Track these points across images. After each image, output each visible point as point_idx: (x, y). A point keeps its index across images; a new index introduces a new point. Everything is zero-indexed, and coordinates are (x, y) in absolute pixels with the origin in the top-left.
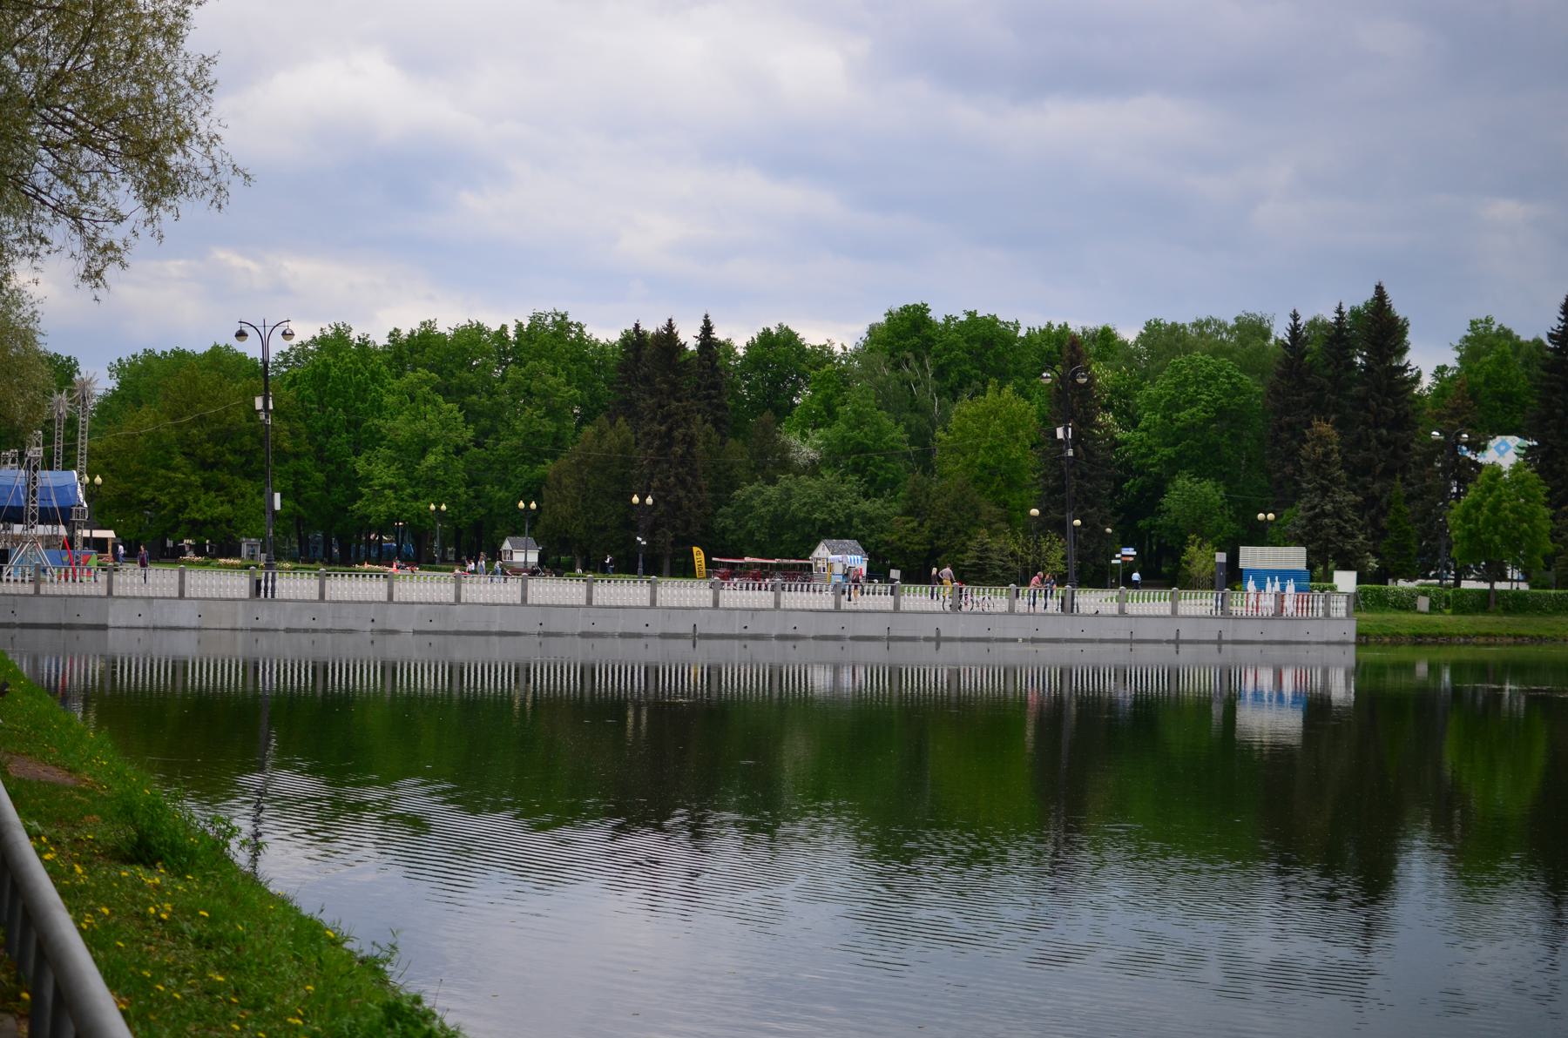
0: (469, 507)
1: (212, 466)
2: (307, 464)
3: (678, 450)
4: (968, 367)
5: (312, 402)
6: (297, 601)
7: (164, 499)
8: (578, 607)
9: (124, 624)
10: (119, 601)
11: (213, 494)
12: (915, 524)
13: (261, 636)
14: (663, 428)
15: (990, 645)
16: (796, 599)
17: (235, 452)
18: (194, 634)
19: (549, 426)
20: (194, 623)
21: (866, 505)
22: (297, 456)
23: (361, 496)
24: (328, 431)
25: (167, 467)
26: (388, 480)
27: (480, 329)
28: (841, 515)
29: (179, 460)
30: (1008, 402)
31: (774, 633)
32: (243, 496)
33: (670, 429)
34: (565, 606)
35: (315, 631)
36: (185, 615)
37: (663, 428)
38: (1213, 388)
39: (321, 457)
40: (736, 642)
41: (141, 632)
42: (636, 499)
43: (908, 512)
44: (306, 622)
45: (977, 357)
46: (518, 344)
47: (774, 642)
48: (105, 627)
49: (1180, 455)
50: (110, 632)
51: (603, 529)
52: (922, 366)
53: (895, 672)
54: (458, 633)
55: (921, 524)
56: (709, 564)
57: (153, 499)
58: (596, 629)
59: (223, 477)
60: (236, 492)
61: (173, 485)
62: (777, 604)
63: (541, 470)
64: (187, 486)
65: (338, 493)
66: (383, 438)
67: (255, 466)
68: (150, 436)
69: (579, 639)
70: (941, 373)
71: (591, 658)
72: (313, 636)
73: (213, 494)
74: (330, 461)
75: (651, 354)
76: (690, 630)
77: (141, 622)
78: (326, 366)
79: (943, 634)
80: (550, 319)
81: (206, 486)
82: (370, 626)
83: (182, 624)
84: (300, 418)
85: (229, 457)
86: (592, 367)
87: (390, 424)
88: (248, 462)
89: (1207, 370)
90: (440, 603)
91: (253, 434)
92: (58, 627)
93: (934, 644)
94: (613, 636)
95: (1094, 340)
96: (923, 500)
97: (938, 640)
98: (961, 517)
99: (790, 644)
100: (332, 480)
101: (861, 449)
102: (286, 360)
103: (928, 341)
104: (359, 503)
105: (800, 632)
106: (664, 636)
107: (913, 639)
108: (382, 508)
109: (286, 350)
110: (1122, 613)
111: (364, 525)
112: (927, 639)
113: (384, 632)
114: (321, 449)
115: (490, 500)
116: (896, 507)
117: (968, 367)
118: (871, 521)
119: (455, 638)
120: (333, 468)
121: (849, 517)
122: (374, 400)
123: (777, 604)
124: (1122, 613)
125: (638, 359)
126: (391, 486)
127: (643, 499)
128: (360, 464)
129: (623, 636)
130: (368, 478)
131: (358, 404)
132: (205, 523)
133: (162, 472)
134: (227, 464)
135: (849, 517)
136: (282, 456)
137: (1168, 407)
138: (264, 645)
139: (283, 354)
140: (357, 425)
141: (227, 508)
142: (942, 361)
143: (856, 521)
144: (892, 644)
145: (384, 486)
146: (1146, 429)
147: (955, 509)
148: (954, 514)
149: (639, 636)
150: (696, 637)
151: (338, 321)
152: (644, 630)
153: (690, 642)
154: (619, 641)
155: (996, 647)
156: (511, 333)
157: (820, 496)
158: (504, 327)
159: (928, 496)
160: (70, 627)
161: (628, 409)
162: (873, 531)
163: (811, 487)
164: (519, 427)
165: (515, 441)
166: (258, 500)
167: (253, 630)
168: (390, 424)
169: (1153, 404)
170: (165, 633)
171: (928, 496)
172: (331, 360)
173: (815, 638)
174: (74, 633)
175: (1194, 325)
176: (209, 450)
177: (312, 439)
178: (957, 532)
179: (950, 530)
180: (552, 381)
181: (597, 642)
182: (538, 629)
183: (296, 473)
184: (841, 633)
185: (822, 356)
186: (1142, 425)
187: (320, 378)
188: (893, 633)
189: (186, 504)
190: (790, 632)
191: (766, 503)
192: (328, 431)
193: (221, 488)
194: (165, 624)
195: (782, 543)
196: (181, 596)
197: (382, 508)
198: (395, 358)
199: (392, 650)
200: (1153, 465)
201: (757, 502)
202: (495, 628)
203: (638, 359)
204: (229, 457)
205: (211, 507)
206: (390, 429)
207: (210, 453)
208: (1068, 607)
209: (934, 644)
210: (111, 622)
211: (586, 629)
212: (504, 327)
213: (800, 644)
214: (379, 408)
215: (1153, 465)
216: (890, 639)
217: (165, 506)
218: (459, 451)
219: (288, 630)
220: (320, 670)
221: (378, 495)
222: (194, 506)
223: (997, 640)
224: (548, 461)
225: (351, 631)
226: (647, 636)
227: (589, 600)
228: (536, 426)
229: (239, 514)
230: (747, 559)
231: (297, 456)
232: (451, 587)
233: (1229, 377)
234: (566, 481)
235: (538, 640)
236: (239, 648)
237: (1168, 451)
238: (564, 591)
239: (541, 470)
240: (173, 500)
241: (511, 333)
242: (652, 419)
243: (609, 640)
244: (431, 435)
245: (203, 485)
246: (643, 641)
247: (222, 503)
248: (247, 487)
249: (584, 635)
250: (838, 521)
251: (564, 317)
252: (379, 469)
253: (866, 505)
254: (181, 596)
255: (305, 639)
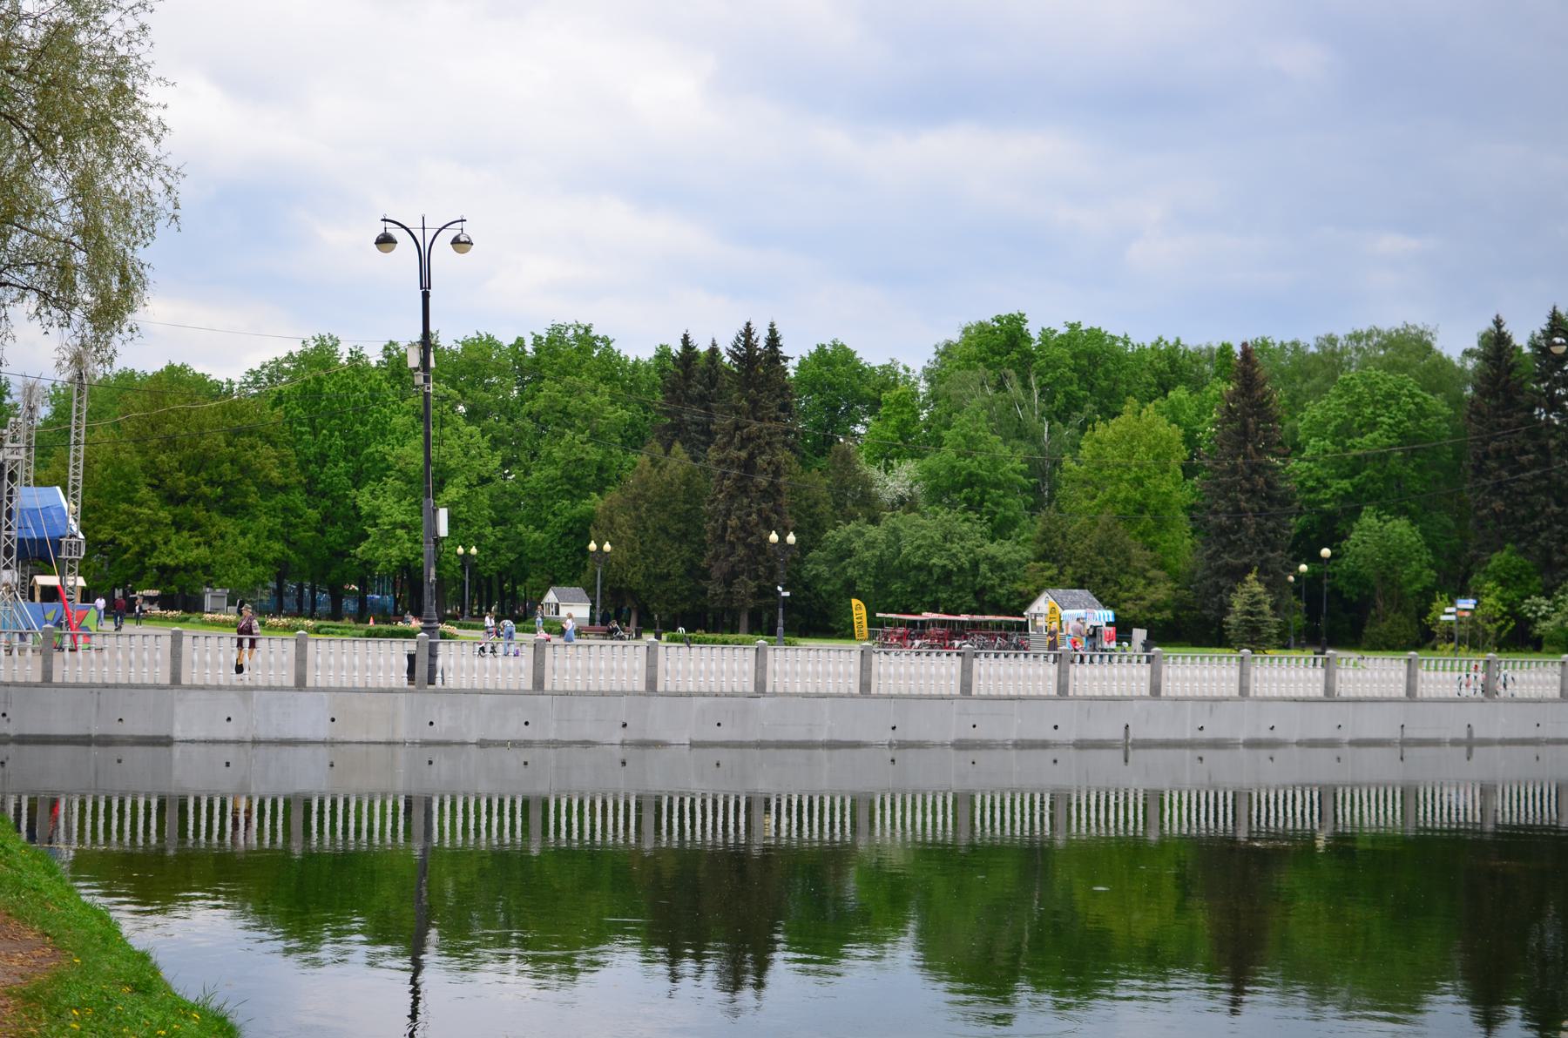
0: (495, 551)
1: (183, 500)
2: (297, 498)
3: (763, 481)
4: (1075, 387)
5: (301, 424)
6: (497, 692)
7: (126, 540)
8: (950, 698)
9: (202, 735)
10: (193, 694)
11: (186, 534)
12: (1055, 571)
13: (438, 754)
14: (743, 454)
15: (1540, 750)
16: (999, 672)
17: (211, 483)
18: (323, 751)
19: (594, 454)
20: (324, 732)
21: (992, 549)
22: (284, 489)
23: (366, 536)
24: (322, 459)
25: (130, 501)
26: (400, 518)
27: (491, 343)
28: (964, 560)
29: (144, 492)
30: (1147, 424)
31: (1242, 736)
32: (222, 537)
33: (751, 456)
34: (931, 697)
35: (527, 744)
36: (307, 718)
37: (743, 454)
38: (1394, 409)
39: (310, 488)
40: (1188, 752)
41: (232, 749)
42: (593, 546)
43: (1042, 557)
44: (513, 731)
45: (1084, 376)
46: (536, 361)
47: (1242, 751)
48: (167, 741)
49: (1359, 489)
50: (177, 750)
51: (666, 577)
52: (1026, 386)
53: (1409, 794)
54: (761, 745)
55: (1061, 573)
56: (873, 622)
57: (112, 541)
58: (980, 734)
59: (199, 514)
60: (214, 532)
61: (138, 523)
62: (1062, 688)
63: (584, 507)
64: (154, 524)
65: (335, 535)
66: (389, 468)
67: (235, 501)
68: (109, 464)
69: (952, 752)
70: (1047, 393)
71: (970, 784)
72: (525, 754)
73: (186, 534)
74: (323, 494)
75: (687, 371)
76: (1119, 734)
77: (230, 732)
78: (318, 380)
79: (1476, 735)
80: (571, 332)
81: (178, 525)
82: (618, 735)
83: (303, 733)
84: (287, 442)
85: (206, 489)
86: (623, 388)
87: (398, 450)
88: (225, 497)
89: (1385, 387)
90: (733, 695)
91: (232, 462)
92: (86, 741)
93: (1464, 750)
94: (1004, 746)
95: (1211, 358)
96: (1060, 542)
97: (1470, 744)
98: (1109, 562)
99: (1264, 753)
100: (327, 518)
101: (971, 480)
102: (257, 380)
103: (1028, 357)
104: (364, 546)
105: (1279, 734)
106: (1081, 745)
107: (1436, 743)
108: (394, 552)
109: (257, 368)
110: (1330, 695)
111: (365, 575)
112: (1455, 743)
113: (644, 744)
114: (313, 480)
115: (521, 543)
116: (1027, 552)
117: (1075, 387)
118: (1001, 567)
119: (757, 752)
120: (329, 503)
121: (975, 564)
122: (377, 421)
123: (1062, 688)
124: (1330, 695)
125: (687, 377)
126: (403, 526)
127: (600, 548)
128: (364, 499)
129: (1020, 745)
130: (373, 517)
131: (358, 427)
132: (177, 569)
133: (123, 506)
134: (204, 497)
135: (975, 564)
136: (268, 489)
137: (1337, 432)
138: (442, 775)
139: (252, 372)
140: (354, 452)
141: (204, 551)
142: (1046, 380)
143: (984, 568)
144: (1408, 751)
145: (395, 525)
146: (1313, 459)
147: (1100, 553)
148: (1101, 560)
149: (1044, 745)
150: (1128, 746)
151: (324, 333)
152: (1051, 735)
153: (1120, 754)
154: (1014, 753)
155: (1547, 752)
156: (529, 347)
157: (937, 536)
158: (520, 341)
159: (1064, 537)
160: (106, 741)
161: (674, 433)
162: (1003, 579)
163: (923, 527)
164: (557, 453)
165: (551, 471)
166: (241, 541)
167: (426, 743)
168: (398, 450)
169: (1318, 428)
170: (273, 750)
171: (1064, 537)
172: (323, 374)
173: (1299, 744)
174: (115, 752)
175: (1351, 338)
176: (181, 481)
177: (304, 465)
178: (1105, 581)
179: (1098, 579)
180: (594, 400)
181: (980, 756)
182: (890, 736)
183: (285, 509)
184: (1336, 734)
185: (888, 378)
186: (1308, 452)
187: (311, 395)
188: (1409, 734)
189: (154, 546)
190: (1265, 734)
191: (870, 545)
192: (322, 459)
193: (195, 526)
194: (273, 735)
195: (891, 594)
196: (300, 683)
197: (394, 552)
198: (393, 375)
199: (657, 777)
200: (1327, 501)
201: (858, 544)
202: (822, 737)
203: (687, 377)
204: (206, 489)
205: (181, 550)
206: (398, 458)
207: (182, 484)
208: (420, 671)
209: (1464, 750)
210: (178, 733)
211: (963, 736)
212: (520, 341)
213: (1279, 753)
214: (382, 431)
215: (1327, 501)
216: (1405, 743)
217: (129, 547)
218: (484, 481)
219: (483, 744)
220: (534, 808)
221: (387, 537)
222: (164, 549)
223: (1550, 742)
224: (594, 494)
225: (586, 744)
226: (1056, 745)
227: (966, 687)
228: (577, 453)
229: (219, 558)
230: (988, 618)
231: (284, 489)
232: (1234, 672)
233: (1412, 395)
234: (621, 519)
235: (889, 754)
236: (401, 778)
237: (1345, 484)
238: (619, 663)
239: (584, 507)
240: (137, 541)
241: (529, 347)
242: (729, 443)
243: (997, 755)
244: (452, 463)
245: (174, 523)
246: (1049, 754)
247: (198, 545)
248: (227, 525)
249: (961, 745)
250: (961, 569)
251: (587, 330)
252: (384, 503)
253: (992, 549)
254: (300, 683)
255: (513, 758)
